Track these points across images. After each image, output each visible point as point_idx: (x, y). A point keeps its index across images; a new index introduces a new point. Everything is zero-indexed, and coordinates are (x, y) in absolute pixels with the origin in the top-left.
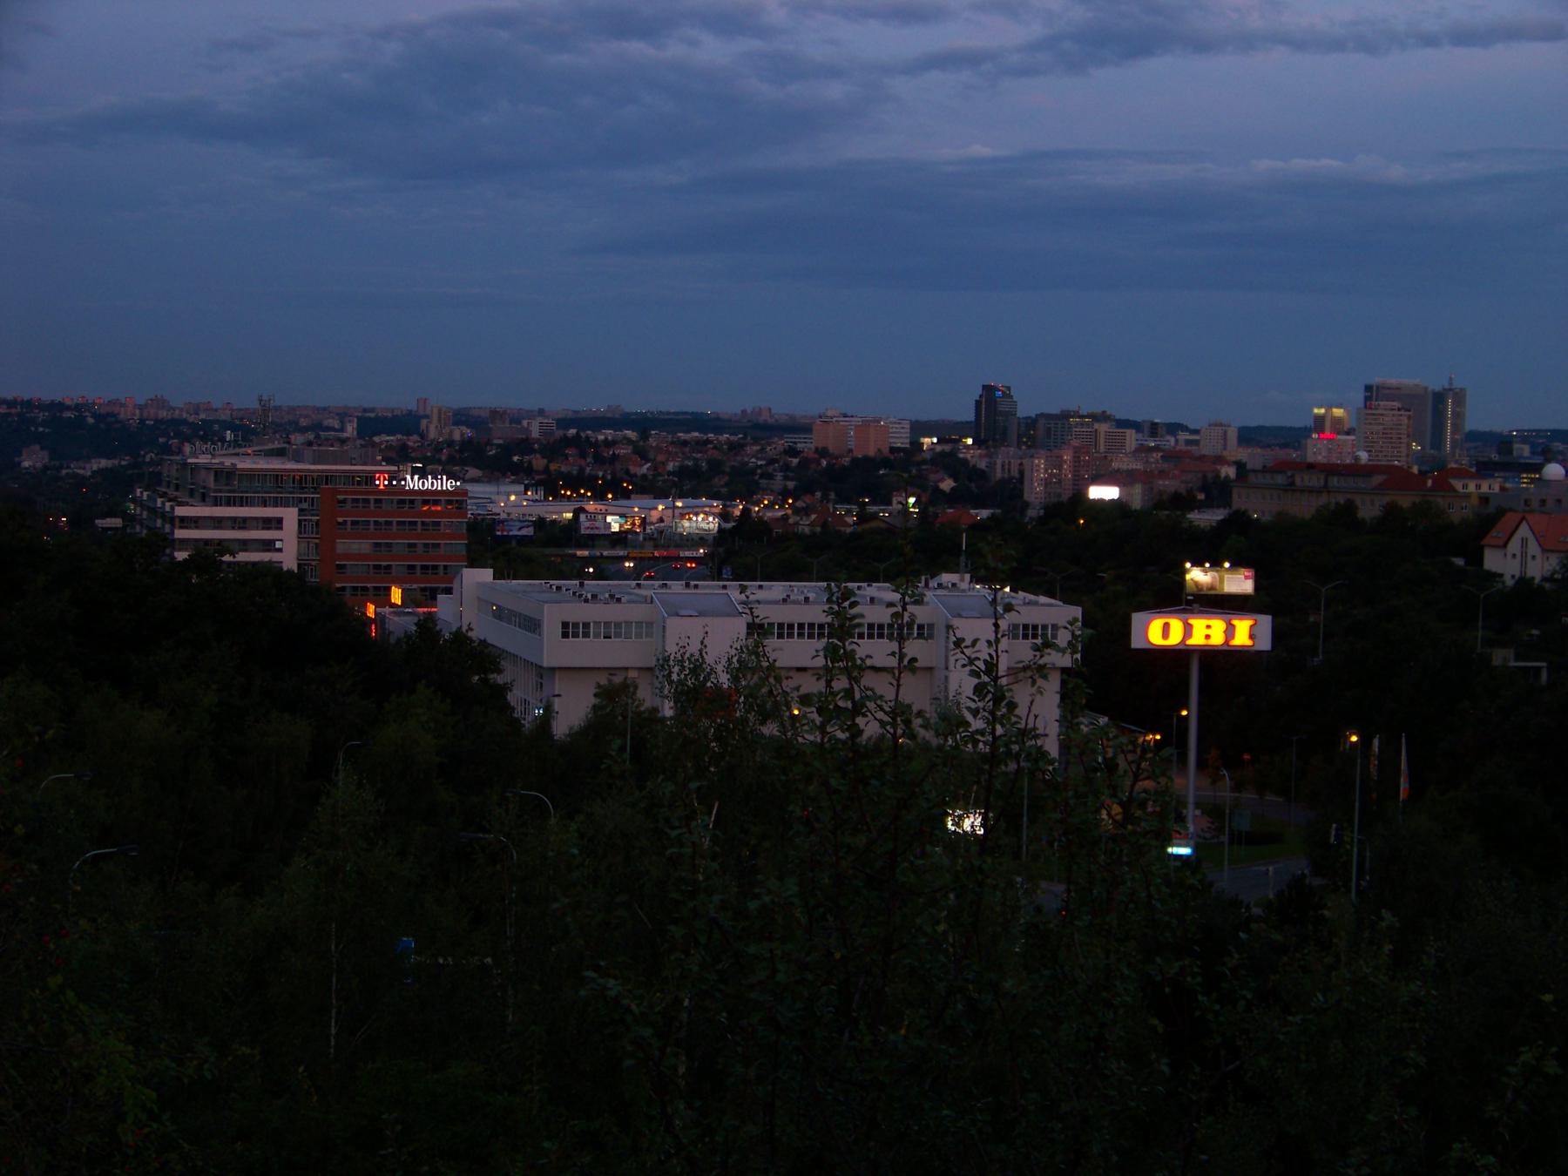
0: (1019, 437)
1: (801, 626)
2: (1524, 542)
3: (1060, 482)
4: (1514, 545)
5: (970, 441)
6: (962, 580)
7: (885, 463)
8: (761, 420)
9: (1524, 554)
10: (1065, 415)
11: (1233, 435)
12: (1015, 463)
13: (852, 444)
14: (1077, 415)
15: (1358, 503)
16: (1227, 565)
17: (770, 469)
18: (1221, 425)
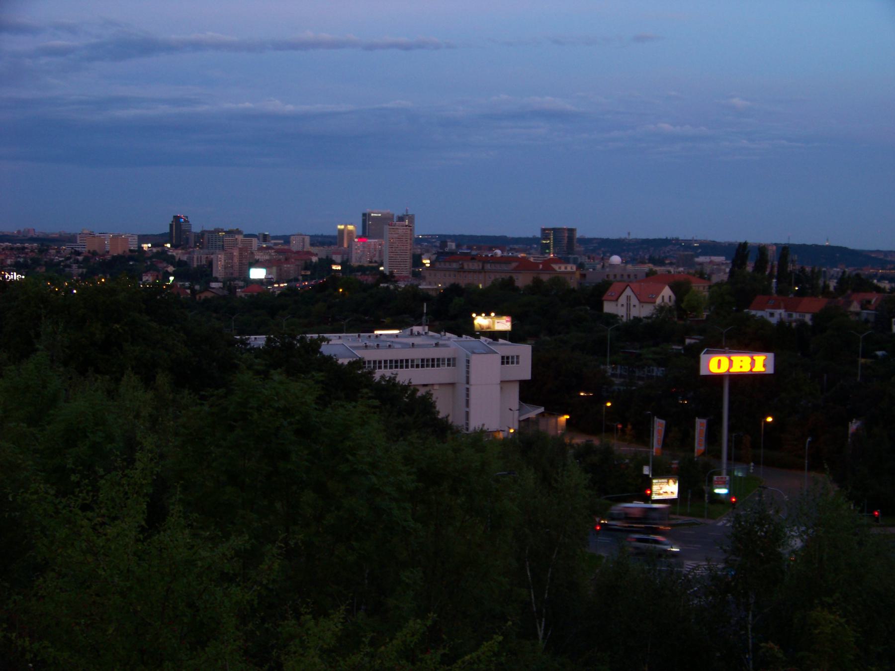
0: (195, 243)
1: (386, 361)
2: (628, 298)
3: (232, 267)
4: (623, 299)
5: (169, 245)
6: (424, 330)
7: (131, 258)
8: (30, 235)
9: (628, 305)
10: (217, 231)
11: (307, 240)
12: (204, 257)
13: (108, 248)
14: (222, 231)
15: (515, 277)
16: (794, 325)
17: (68, 262)
18: (301, 235)
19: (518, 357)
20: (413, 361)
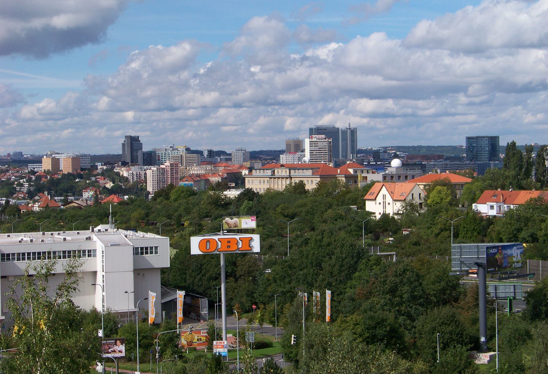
1: (29, 254)
2: (384, 197)
4: (380, 198)
9: (384, 203)
15: (305, 182)
19: (156, 248)
20: (54, 253)
